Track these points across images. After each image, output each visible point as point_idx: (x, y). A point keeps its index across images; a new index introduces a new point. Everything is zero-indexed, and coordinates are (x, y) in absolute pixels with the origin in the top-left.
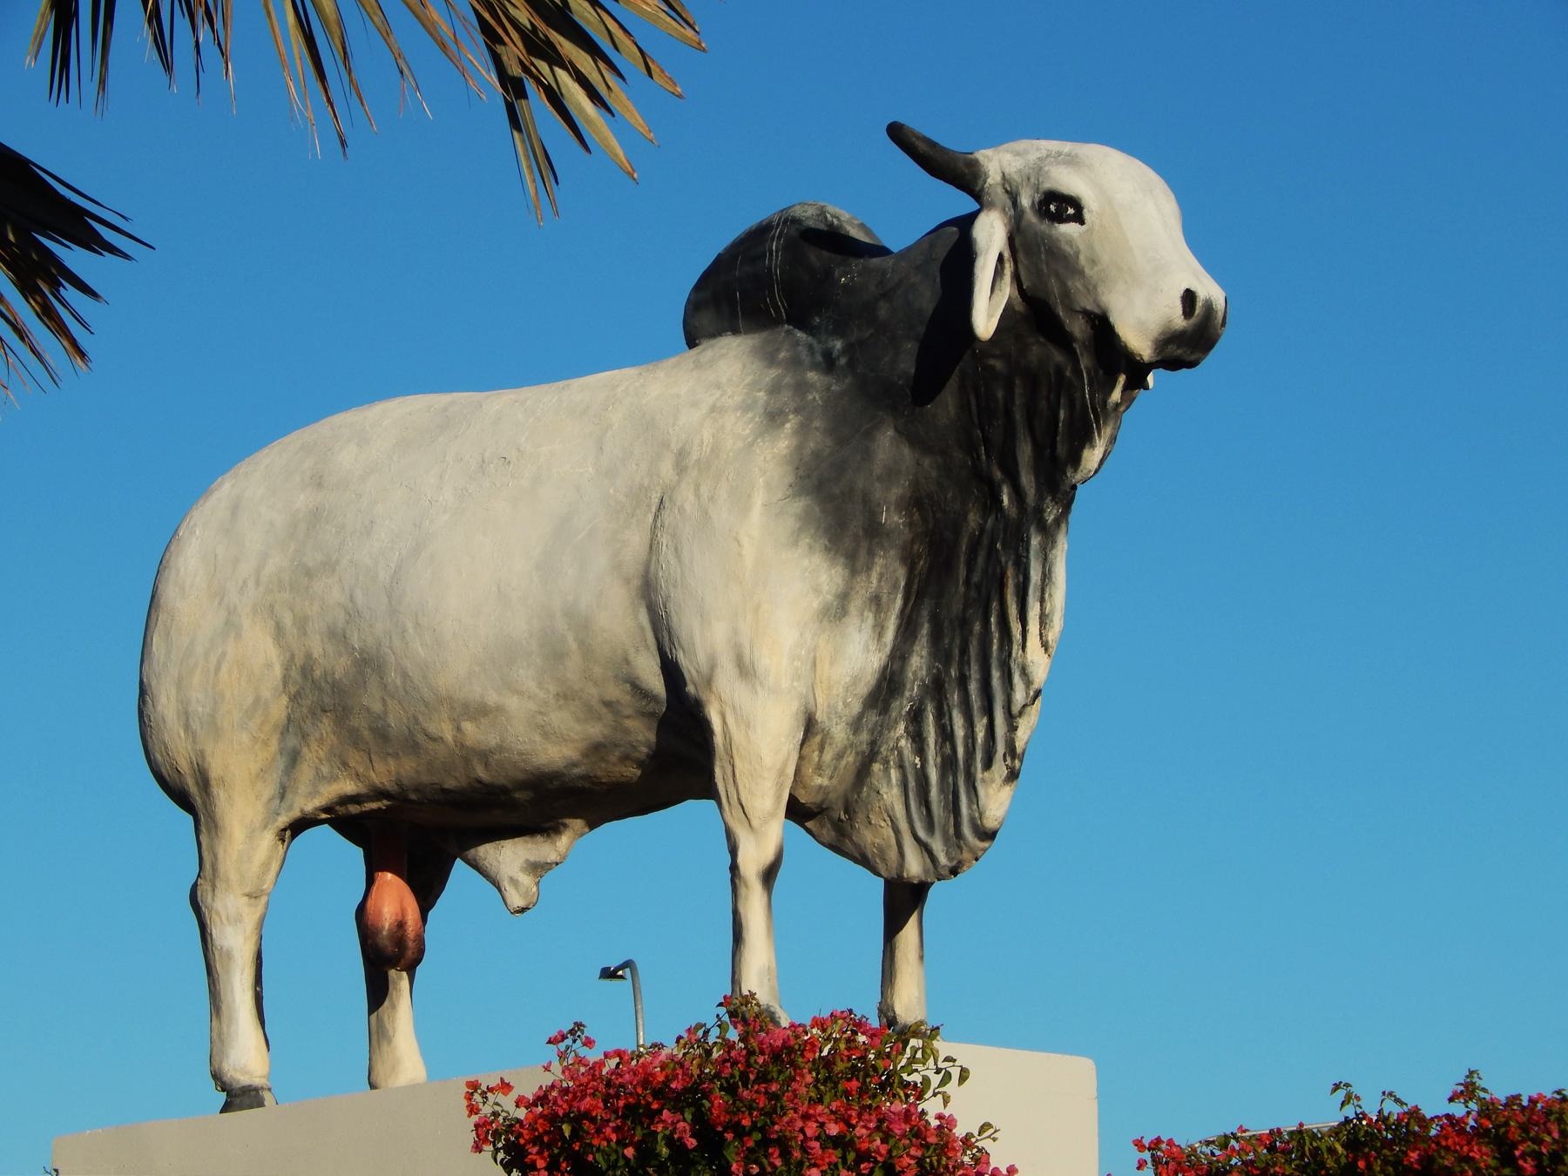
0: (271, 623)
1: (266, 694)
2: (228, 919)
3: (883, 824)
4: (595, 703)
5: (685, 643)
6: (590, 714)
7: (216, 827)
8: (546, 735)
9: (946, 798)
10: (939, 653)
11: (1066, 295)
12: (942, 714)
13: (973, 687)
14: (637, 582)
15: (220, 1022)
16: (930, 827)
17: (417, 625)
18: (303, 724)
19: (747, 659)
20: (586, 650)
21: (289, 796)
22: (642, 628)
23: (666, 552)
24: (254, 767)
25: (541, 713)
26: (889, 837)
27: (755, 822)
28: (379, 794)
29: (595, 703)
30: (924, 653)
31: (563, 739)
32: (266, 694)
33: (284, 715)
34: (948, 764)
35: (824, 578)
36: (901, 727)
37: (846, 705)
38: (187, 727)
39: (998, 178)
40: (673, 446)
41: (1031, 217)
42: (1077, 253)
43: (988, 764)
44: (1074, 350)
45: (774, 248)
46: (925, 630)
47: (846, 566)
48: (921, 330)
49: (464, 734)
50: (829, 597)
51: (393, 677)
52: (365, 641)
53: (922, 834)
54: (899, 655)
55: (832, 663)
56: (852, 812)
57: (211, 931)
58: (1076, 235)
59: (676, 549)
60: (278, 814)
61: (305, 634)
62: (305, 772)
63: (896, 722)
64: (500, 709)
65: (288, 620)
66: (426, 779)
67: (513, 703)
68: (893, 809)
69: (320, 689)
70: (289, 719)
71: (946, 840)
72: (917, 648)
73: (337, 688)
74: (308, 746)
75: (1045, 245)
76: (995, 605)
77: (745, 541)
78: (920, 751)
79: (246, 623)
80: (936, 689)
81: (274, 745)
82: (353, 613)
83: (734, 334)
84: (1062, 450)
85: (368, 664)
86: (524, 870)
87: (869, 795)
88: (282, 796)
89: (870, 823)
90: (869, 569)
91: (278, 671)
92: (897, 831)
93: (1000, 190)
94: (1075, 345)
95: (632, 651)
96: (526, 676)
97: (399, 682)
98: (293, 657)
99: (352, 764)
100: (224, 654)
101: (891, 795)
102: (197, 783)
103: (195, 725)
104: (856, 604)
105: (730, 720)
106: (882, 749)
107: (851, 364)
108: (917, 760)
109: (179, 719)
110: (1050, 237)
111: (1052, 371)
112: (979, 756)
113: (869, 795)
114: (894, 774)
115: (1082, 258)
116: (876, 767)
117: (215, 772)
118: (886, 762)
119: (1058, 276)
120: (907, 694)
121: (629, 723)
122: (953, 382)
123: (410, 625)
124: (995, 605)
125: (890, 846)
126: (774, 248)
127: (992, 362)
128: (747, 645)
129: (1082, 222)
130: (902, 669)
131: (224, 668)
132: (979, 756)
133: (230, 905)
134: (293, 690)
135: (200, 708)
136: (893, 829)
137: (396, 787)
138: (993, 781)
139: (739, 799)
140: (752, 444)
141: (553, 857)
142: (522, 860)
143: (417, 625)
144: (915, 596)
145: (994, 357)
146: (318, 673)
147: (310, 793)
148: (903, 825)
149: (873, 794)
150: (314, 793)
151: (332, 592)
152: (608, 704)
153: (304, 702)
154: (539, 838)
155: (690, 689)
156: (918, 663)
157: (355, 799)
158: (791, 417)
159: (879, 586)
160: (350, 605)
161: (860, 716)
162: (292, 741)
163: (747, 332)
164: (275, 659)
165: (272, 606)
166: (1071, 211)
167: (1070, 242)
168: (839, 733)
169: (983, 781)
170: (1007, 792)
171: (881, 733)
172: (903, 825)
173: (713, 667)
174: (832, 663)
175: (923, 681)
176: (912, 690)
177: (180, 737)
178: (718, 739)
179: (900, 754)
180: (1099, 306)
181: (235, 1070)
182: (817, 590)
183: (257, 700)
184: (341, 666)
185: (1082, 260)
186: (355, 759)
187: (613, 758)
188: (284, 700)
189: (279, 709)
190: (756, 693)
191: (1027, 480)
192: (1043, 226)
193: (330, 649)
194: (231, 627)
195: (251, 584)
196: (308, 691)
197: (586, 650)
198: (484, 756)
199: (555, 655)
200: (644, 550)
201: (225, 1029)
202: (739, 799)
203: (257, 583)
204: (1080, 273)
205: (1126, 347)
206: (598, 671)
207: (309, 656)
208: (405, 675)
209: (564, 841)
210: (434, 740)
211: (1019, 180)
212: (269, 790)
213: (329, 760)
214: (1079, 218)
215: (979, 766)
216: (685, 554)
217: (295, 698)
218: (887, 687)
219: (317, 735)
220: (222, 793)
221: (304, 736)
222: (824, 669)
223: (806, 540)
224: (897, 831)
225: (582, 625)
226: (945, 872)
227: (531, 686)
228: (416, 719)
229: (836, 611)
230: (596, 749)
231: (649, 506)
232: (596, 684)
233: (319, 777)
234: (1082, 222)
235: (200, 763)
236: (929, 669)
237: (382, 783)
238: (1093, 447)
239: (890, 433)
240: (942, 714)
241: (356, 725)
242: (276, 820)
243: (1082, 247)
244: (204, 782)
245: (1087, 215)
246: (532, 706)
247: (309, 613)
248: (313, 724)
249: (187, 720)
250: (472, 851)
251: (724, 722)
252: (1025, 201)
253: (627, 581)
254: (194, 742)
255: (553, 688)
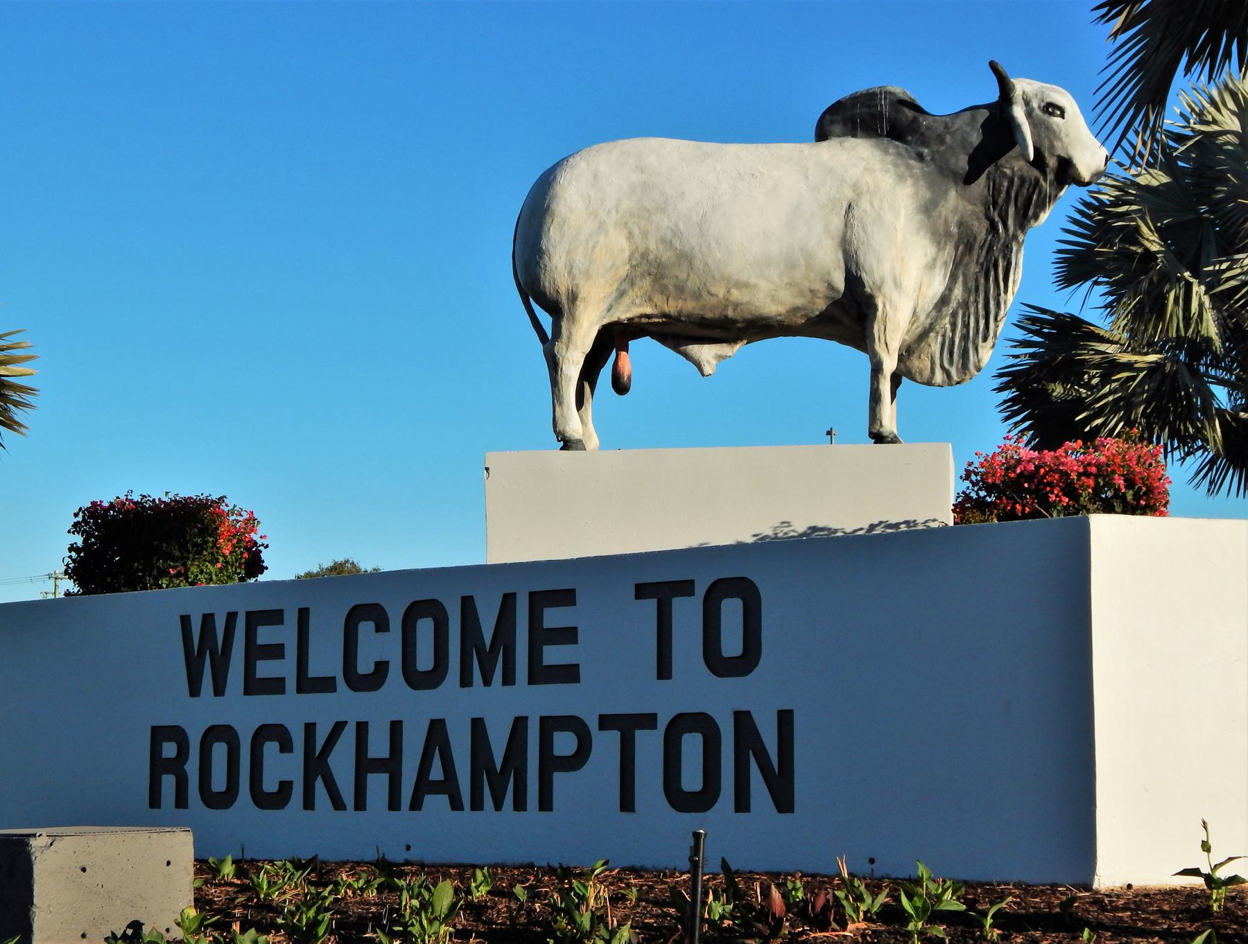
0: (626, 232)
1: (618, 263)
2: (573, 362)
3: (927, 359)
4: (805, 289)
5: (867, 267)
6: (801, 293)
7: (574, 319)
8: (773, 300)
9: (960, 351)
10: (967, 290)
11: (1052, 147)
12: (966, 316)
13: (981, 306)
14: (838, 240)
15: (562, 409)
16: (951, 362)
17: (717, 242)
18: (634, 279)
19: (898, 281)
20: (809, 267)
21: (613, 310)
22: (839, 261)
23: (857, 229)
24: (602, 295)
25: (775, 290)
26: (928, 365)
27: (890, 351)
28: (665, 315)
29: (805, 289)
30: (961, 289)
31: (781, 303)
32: (618, 263)
33: (626, 274)
34: (965, 337)
35: (929, 250)
36: (947, 320)
37: (928, 306)
38: (570, 273)
39: (1021, 93)
40: (849, 181)
41: (1038, 112)
42: (1061, 131)
43: (985, 339)
44: (1046, 171)
45: (883, 103)
46: (961, 279)
47: (936, 247)
48: (971, 151)
49: (731, 294)
50: (930, 259)
51: (698, 264)
52: (684, 246)
53: (946, 365)
54: (950, 288)
55: (928, 288)
56: (912, 352)
57: (562, 366)
58: (1061, 123)
59: (863, 227)
60: (604, 318)
61: (647, 238)
62: (626, 300)
63: (945, 316)
64: (755, 286)
65: (636, 232)
66: (697, 312)
67: (763, 284)
68: (935, 354)
69: (651, 265)
70: (627, 276)
71: (957, 369)
72: (957, 286)
73: (660, 265)
74: (633, 289)
75: (1044, 125)
76: (992, 273)
77: (898, 229)
78: (953, 330)
79: (611, 229)
80: (965, 305)
81: (615, 287)
82: (676, 232)
83: (852, 137)
84: (1031, 212)
85: (685, 257)
86: (714, 358)
87: (924, 346)
88: (609, 310)
89: (920, 358)
90: (945, 249)
91: (627, 254)
92: (933, 363)
93: (1021, 98)
94: (1048, 170)
95: (832, 269)
96: (774, 274)
97: (701, 267)
98: (637, 248)
99: (655, 300)
100: (597, 242)
101: (936, 348)
102: (568, 299)
103: (575, 271)
104: (939, 263)
105: (887, 306)
106: (937, 327)
107: (933, 159)
108: (951, 334)
109: (565, 268)
110: (1048, 122)
111: (1033, 178)
112: (981, 335)
113: (924, 346)
114: (940, 339)
115: (1062, 133)
116: (932, 335)
117: (582, 294)
118: (938, 333)
119: (1049, 139)
120: (951, 305)
121: (818, 301)
122: (984, 176)
123: (713, 243)
124: (992, 273)
125: (927, 369)
126: (883, 103)
127: (1005, 170)
128: (898, 276)
129: (1064, 118)
130: (950, 295)
131: (598, 248)
132: (981, 335)
133: (575, 356)
134: (634, 263)
135: (580, 261)
136: (931, 362)
137: (676, 313)
138: (986, 347)
139: (885, 340)
140: (894, 187)
141: (730, 354)
142: (714, 353)
143: (717, 242)
144: (957, 264)
145: (1006, 168)
146: (651, 257)
147: (625, 311)
148: (938, 361)
149: (927, 346)
150: (626, 312)
151: (664, 223)
152: (811, 291)
153: (639, 269)
154: (724, 345)
155: (868, 290)
156: (958, 292)
157: (648, 316)
158: (908, 178)
159: (947, 258)
160: (675, 229)
161: (930, 312)
162: (625, 286)
163: (861, 137)
164: (626, 247)
165: (626, 223)
166: (1058, 112)
167: (1058, 126)
168: (922, 317)
169: (982, 346)
170: (991, 352)
171: (936, 320)
172: (938, 361)
173: (883, 282)
174: (928, 288)
175: (959, 301)
176: (953, 304)
177: (564, 275)
178: (879, 313)
179: (945, 331)
180: (1068, 155)
181: (573, 431)
182: (926, 255)
183: (613, 265)
184: (667, 256)
185: (1062, 135)
186: (658, 299)
187: (799, 315)
188: (628, 267)
189: (624, 270)
190: (901, 296)
191: (1010, 222)
192: (1046, 117)
193: (661, 247)
194: (601, 227)
195: (614, 211)
196: (643, 265)
197: (809, 267)
198: (736, 306)
199: (791, 265)
200: (842, 226)
201: (565, 411)
202: (885, 340)
203: (617, 212)
204: (1061, 140)
205: (1079, 174)
206: (812, 275)
207: (647, 249)
208: (706, 264)
209: (737, 347)
210: (712, 295)
211: (1031, 95)
212: (604, 306)
213: (641, 297)
214: (1062, 115)
215: (980, 340)
216: (869, 232)
217: (633, 267)
218: (944, 301)
219: (640, 285)
220: (582, 305)
221: (632, 284)
222: (924, 290)
223: (922, 233)
224: (933, 363)
225: (809, 257)
226: (954, 383)
227: (776, 279)
228: (705, 285)
229: (931, 266)
230: (795, 310)
231: (842, 207)
232: (809, 282)
233: (633, 303)
234: (1064, 118)
235: (574, 289)
236: (962, 296)
237: (670, 311)
238: (1045, 212)
239: (954, 192)
240: (966, 316)
241: (667, 283)
242: (602, 320)
243: (1063, 129)
244: (573, 297)
245: (1066, 115)
246: (773, 287)
247: (650, 229)
248: (640, 280)
249: (572, 268)
250: (690, 347)
251: (884, 306)
252: (1035, 104)
253: (833, 238)
254: (573, 279)
255: (786, 280)
